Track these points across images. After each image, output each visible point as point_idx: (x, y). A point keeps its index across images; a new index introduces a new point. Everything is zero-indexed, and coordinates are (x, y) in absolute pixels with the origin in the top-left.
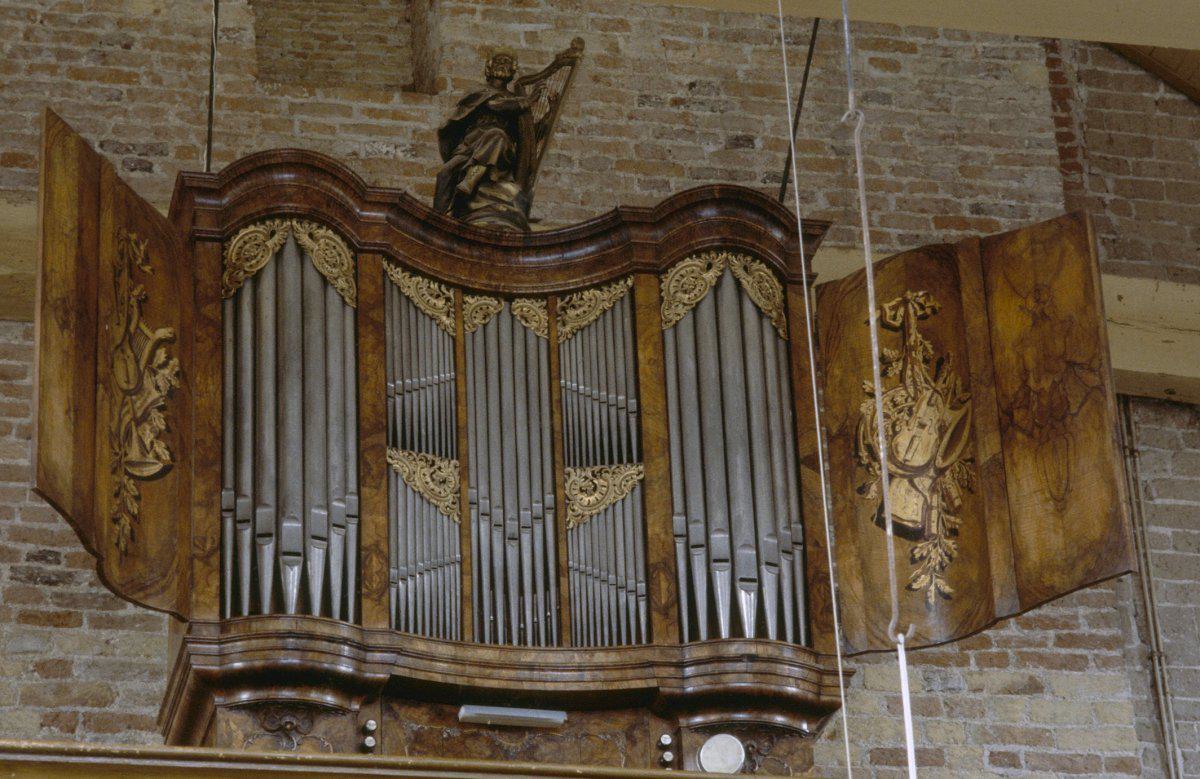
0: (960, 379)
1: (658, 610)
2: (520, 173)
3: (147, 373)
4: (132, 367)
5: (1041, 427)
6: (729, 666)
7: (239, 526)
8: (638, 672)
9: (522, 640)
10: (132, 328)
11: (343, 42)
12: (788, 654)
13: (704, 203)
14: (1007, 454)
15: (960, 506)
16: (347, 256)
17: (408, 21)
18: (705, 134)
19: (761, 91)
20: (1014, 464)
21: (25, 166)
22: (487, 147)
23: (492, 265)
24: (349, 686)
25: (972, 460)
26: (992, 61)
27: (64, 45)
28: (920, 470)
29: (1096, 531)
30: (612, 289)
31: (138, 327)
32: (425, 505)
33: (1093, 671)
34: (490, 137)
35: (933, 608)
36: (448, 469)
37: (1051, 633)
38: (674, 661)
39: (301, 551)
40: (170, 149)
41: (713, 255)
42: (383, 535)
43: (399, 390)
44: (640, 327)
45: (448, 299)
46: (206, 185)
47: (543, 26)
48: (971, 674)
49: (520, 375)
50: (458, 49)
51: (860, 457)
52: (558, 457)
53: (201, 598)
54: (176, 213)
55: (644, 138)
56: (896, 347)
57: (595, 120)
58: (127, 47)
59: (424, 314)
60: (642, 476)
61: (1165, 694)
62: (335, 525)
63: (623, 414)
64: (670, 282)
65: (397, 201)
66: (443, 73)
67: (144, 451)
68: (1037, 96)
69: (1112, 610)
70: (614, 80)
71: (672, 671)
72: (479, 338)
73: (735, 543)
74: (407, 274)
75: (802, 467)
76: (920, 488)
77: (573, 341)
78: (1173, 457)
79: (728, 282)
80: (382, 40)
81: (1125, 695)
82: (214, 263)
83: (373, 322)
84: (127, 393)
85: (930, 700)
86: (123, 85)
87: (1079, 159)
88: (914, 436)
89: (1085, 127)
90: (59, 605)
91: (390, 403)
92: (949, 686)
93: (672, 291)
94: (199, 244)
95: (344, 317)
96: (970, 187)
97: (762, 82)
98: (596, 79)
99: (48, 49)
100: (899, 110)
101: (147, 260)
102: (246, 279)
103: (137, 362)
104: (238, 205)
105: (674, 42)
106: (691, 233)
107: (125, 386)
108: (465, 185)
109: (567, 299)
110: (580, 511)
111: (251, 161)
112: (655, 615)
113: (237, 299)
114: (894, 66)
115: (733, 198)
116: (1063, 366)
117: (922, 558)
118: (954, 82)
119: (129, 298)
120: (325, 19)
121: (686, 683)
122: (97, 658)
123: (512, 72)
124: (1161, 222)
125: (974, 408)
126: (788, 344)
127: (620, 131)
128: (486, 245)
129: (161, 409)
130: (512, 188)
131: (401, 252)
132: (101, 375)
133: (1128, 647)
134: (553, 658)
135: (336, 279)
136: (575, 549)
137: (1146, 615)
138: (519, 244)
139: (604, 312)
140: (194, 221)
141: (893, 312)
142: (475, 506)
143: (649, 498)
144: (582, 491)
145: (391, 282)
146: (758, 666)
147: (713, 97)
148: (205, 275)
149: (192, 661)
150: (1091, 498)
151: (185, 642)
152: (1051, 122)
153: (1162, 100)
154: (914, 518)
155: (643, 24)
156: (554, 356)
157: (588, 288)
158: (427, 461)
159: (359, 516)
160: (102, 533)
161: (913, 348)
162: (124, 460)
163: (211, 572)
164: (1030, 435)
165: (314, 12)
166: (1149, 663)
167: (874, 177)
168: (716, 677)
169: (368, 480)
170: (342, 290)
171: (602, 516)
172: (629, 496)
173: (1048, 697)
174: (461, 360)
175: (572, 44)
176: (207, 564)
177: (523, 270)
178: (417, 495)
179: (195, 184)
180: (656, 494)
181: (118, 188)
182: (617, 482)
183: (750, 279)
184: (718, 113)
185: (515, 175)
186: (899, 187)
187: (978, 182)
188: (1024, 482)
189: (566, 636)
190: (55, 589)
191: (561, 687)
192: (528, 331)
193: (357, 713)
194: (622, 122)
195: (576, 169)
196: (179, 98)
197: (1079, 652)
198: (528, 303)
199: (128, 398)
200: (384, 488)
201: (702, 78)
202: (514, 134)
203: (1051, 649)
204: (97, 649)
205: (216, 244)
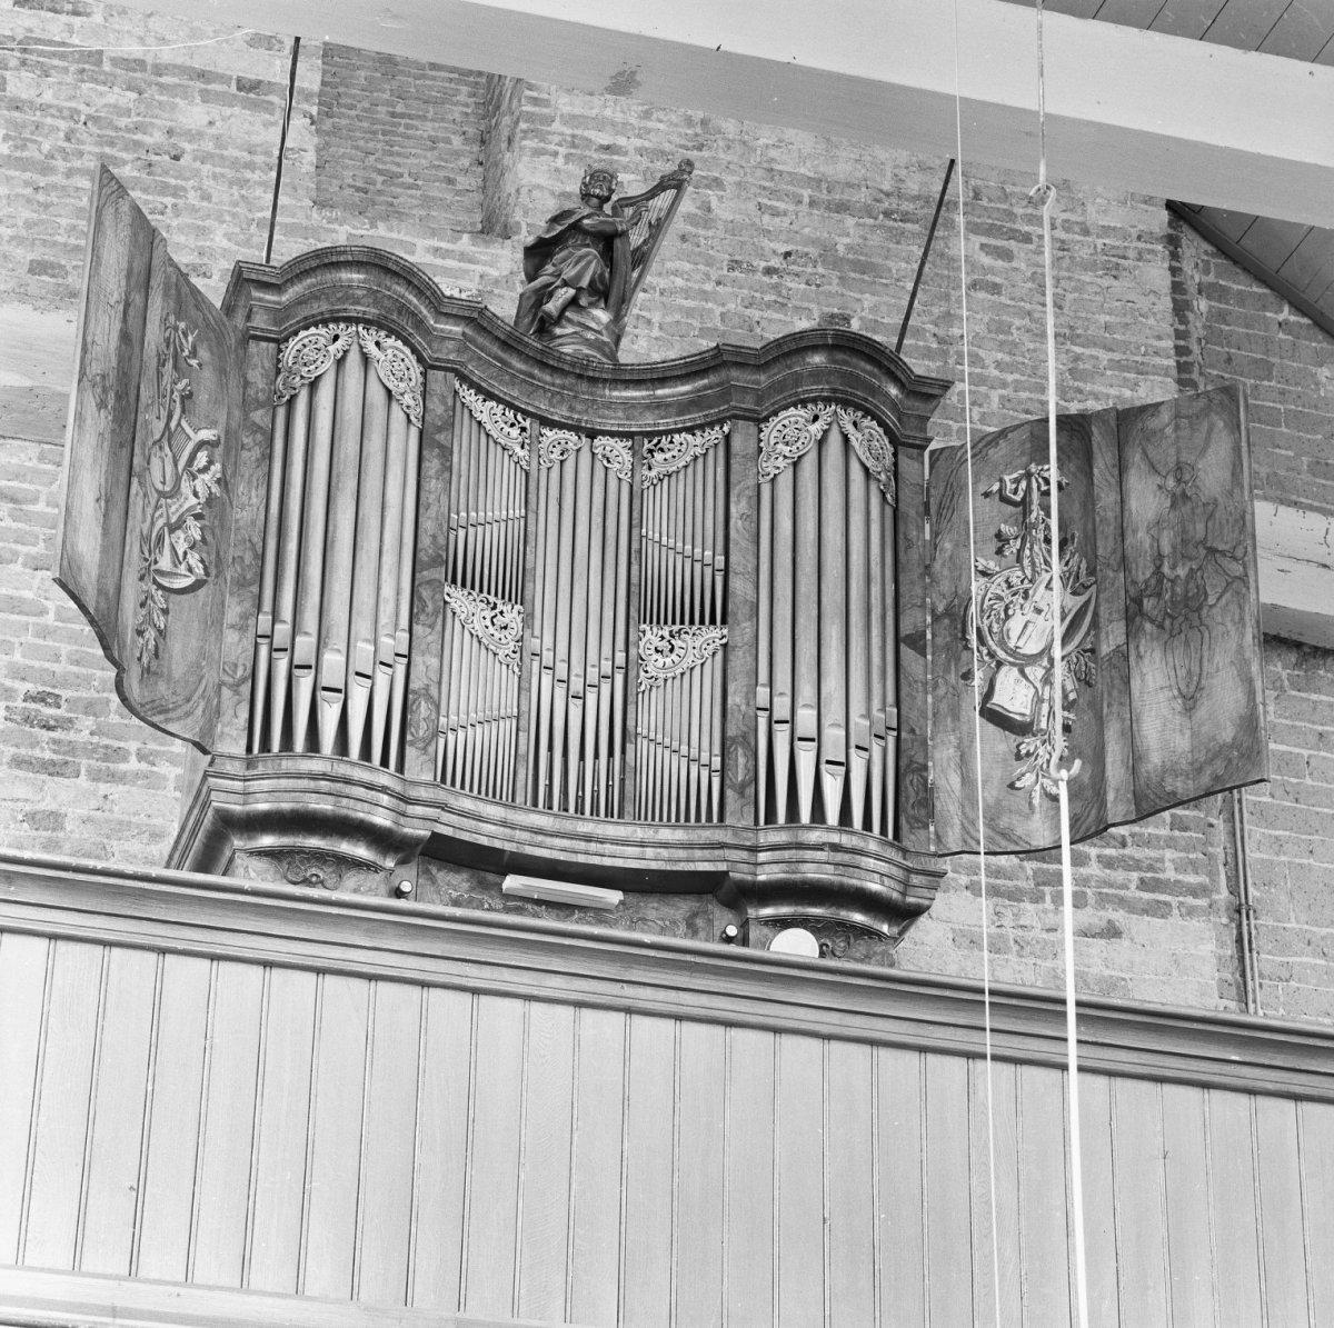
0: (1084, 561)
1: (732, 787)
2: (612, 300)
3: (185, 477)
4: (169, 469)
5: (1173, 618)
6: (809, 854)
7: (275, 655)
8: (707, 853)
9: (580, 809)
10: (173, 425)
11: (408, 180)
12: (873, 846)
13: (815, 348)
14: (1132, 646)
15: (1074, 700)
16: (416, 370)
17: (481, 164)
18: (796, 308)
19: (863, 268)
20: (1139, 657)
21: (53, 276)
22: (578, 267)
23: (575, 397)
24: (382, 839)
25: (1092, 651)
26: (1113, 259)
27: (107, 150)
28: (1033, 659)
29: (1227, 734)
30: (706, 434)
31: (179, 424)
32: (483, 651)
33: (1175, 918)
34: (581, 258)
35: (1037, 810)
36: (512, 615)
37: (1135, 875)
38: (748, 844)
39: (342, 687)
40: (215, 272)
41: (821, 406)
42: (436, 679)
43: (463, 523)
44: (733, 479)
45: (523, 429)
46: (265, 279)
47: (632, 177)
48: (1045, 911)
49: (597, 520)
50: (536, 193)
51: (967, 640)
52: (634, 613)
53: (226, 730)
54: (229, 308)
55: (731, 306)
56: (1016, 523)
57: (679, 282)
58: (176, 158)
59: (496, 443)
60: (724, 641)
61: (1250, 951)
62: (382, 663)
63: (708, 571)
64: (771, 431)
65: (475, 315)
66: (518, 216)
67: (176, 561)
68: (1156, 301)
69: (1201, 856)
70: (703, 241)
71: (744, 855)
72: (555, 474)
73: (823, 721)
74: (481, 397)
75: (903, 647)
76: (1032, 678)
77: (658, 488)
78: (1276, 698)
79: (835, 440)
80: (450, 181)
81: (1208, 948)
82: (267, 365)
83: (441, 446)
84: (161, 494)
85: (1001, 936)
86: (169, 199)
87: (1195, 376)
88: (1028, 622)
89: (1203, 342)
90: (55, 752)
91: (452, 537)
92: (1022, 923)
93: (772, 442)
94: (252, 344)
95: (408, 435)
96: (1080, 391)
97: (862, 258)
98: (683, 238)
99: (89, 153)
100: (1009, 302)
101: (194, 353)
102: (303, 385)
103: (176, 464)
104: (300, 303)
105: (770, 207)
106: (798, 379)
107: (160, 487)
108: (552, 307)
109: (655, 441)
110: (654, 674)
111: (317, 256)
112: (729, 793)
113: (291, 403)
114: (1007, 255)
115: (845, 344)
116: (1203, 552)
117: (1028, 754)
118: (1070, 278)
119: (172, 392)
120: (391, 154)
121: (759, 870)
122: (92, 813)
123: (612, 191)
124: (1277, 450)
125: (1098, 592)
126: (896, 511)
127: (705, 296)
128: (568, 373)
129: (198, 517)
130: (602, 316)
131: (477, 373)
132: (136, 468)
133: (1215, 897)
134: (611, 830)
135: (402, 394)
136: (646, 715)
137: (1237, 865)
138: (605, 376)
139: (696, 458)
140: (248, 318)
141: (1014, 486)
142: (537, 658)
143: (731, 664)
144: (657, 651)
145: (463, 404)
146: (839, 857)
147: (809, 270)
148: (257, 377)
149: (212, 798)
150: (1224, 700)
151: (206, 776)
152: (1170, 331)
153: (1286, 322)
154: (1023, 711)
155: (739, 184)
156: (636, 502)
157: (679, 431)
158: (488, 603)
159: (409, 656)
160: (124, 642)
161: (1034, 526)
162: (153, 567)
163: (239, 702)
164: (1161, 626)
165: (379, 146)
166: (1236, 916)
167: (978, 370)
168: (793, 866)
169: (422, 617)
170: (408, 407)
171: (677, 682)
172: (709, 661)
173: (1126, 943)
174: (532, 497)
175: (680, 166)
176: (237, 693)
177: (609, 405)
178: (475, 639)
179: (254, 276)
180: (739, 661)
181: (170, 269)
182: (697, 645)
183: (859, 435)
184: (813, 287)
185: (606, 302)
186: (1004, 385)
187: (1088, 387)
188: (1149, 678)
189: (629, 807)
190: (52, 734)
191: (619, 863)
192: (610, 472)
193: (391, 872)
194: (708, 287)
195: (656, 333)
196: (228, 218)
197: (1162, 897)
198: (612, 441)
199: (163, 501)
200: (439, 627)
201: (799, 248)
202: (608, 254)
203: (1133, 893)
204: (94, 804)
205: (272, 345)
